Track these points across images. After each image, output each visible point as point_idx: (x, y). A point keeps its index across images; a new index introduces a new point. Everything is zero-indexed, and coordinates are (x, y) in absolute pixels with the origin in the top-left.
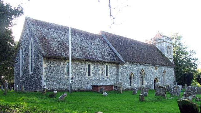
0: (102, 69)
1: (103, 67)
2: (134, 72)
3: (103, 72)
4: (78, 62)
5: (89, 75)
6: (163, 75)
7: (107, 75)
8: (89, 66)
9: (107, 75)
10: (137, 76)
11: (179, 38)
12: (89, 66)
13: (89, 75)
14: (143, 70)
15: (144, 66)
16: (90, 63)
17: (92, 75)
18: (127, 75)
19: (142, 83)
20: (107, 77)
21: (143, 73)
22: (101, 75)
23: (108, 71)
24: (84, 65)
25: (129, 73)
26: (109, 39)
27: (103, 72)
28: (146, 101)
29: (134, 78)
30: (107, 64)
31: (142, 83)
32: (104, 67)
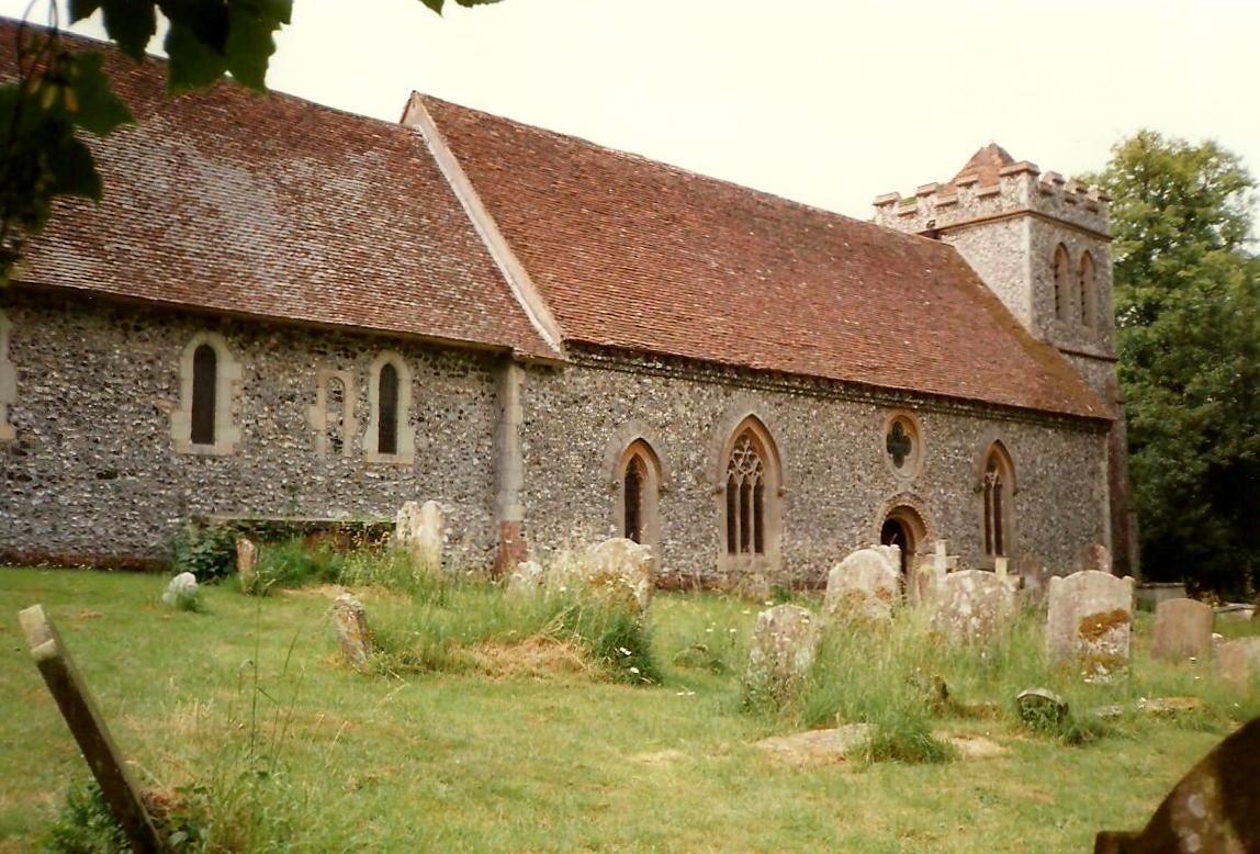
0: (338, 397)
1: (347, 376)
2: (668, 444)
3: (352, 425)
4: (90, 324)
5: (203, 429)
6: (977, 490)
7: (387, 443)
8: (389, 379)
9: (387, 443)
10: (700, 477)
11: (1238, 183)
12: (389, 379)
13: (203, 429)
14: (760, 423)
15: (779, 398)
16: (219, 344)
17: (227, 435)
18: (590, 459)
19: (1022, 580)
20: (387, 458)
21: (763, 454)
22: (323, 442)
23: (403, 415)
24: (149, 350)
25: (615, 444)
26: (442, 124)
27: (352, 425)
28: (1119, 734)
29: (662, 491)
30: (386, 357)
31: (1022, 580)
32: (360, 384)
